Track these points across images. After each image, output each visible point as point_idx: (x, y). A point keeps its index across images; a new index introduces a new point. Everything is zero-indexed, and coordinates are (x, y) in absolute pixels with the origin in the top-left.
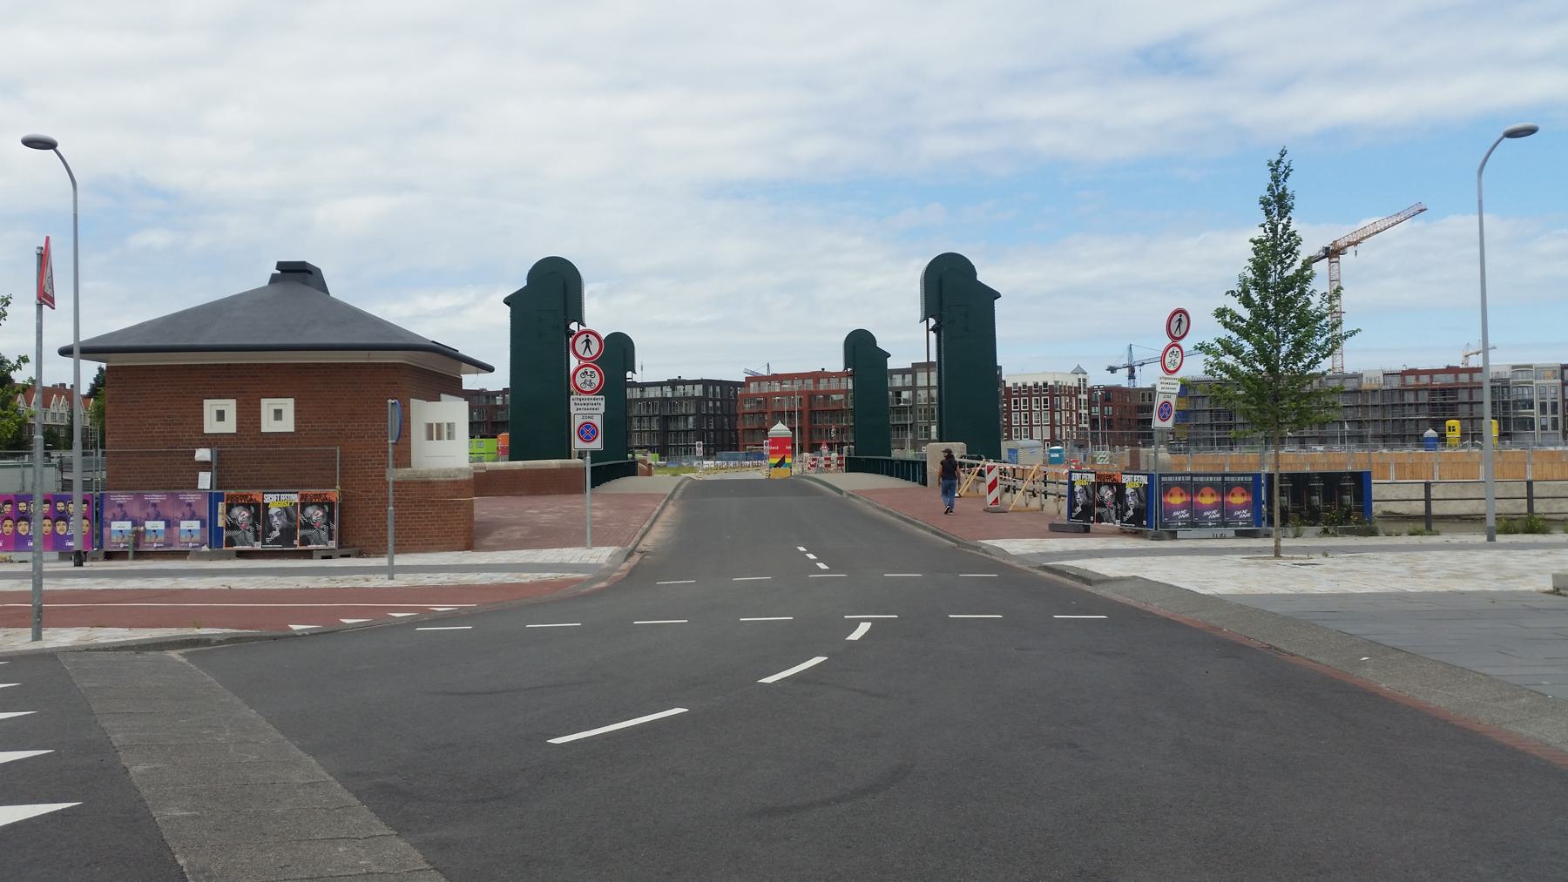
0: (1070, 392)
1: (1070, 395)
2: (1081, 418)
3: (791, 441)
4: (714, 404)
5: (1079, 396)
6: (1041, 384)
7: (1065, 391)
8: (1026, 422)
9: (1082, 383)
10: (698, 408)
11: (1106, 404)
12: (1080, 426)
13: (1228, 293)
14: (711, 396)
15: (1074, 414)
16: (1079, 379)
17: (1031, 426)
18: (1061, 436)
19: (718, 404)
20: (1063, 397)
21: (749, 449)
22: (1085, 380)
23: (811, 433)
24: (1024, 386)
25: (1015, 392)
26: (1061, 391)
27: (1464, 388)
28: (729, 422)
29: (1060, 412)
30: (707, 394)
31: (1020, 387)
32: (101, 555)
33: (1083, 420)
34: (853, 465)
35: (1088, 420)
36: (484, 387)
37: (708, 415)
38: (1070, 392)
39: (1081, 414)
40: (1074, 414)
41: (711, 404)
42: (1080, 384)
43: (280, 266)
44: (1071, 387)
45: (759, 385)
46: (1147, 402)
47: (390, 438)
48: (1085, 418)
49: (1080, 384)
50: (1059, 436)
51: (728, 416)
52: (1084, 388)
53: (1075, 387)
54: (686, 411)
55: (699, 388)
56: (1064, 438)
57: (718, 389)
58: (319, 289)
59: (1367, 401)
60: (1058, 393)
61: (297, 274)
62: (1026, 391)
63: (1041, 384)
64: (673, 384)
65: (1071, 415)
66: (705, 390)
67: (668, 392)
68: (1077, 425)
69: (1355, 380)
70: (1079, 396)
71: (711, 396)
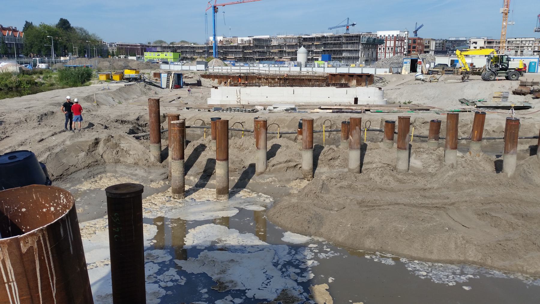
6: (391, 35)
24: (393, 36)
31: (391, 37)
38: (402, 39)
46: (428, 44)
62: (393, 38)
63: (391, 35)
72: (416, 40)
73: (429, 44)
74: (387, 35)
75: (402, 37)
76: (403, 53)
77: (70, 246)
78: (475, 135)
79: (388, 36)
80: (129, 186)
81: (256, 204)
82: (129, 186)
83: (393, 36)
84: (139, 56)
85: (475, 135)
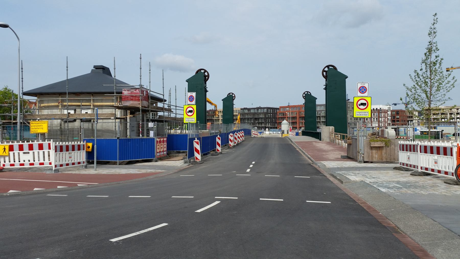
1: (385, 112)
2: (388, 120)
4: (270, 115)
5: (388, 113)
6: (375, 109)
7: (383, 111)
9: (389, 108)
10: (265, 116)
11: (394, 115)
14: (269, 112)
16: (388, 107)
17: (372, 122)
18: (382, 125)
19: (271, 115)
23: (299, 123)
24: (377, 109)
27: (97, 112)
28: (275, 120)
29: (381, 118)
30: (268, 111)
31: (375, 110)
33: (389, 120)
34: (304, 133)
35: (391, 120)
36: (402, 109)
37: (268, 118)
38: (385, 111)
39: (388, 118)
41: (269, 115)
42: (388, 109)
43: (95, 67)
44: (385, 110)
47: (203, 124)
48: (390, 120)
49: (388, 109)
50: (381, 125)
51: (274, 118)
52: (390, 110)
54: (262, 116)
55: (265, 110)
56: (383, 126)
57: (271, 110)
58: (108, 74)
59: (245, 117)
61: (104, 70)
63: (375, 109)
64: (258, 109)
65: (385, 119)
66: (268, 110)
67: (256, 111)
70: (388, 113)
71: (269, 112)
72: (399, 111)
73: (286, 116)
74: (379, 108)
75: (385, 110)
76: (387, 122)
77: (72, 174)
78: (165, 171)
79: (373, 109)
80: (21, 169)
81: (398, 159)
82: (21, 169)
83: (377, 109)
84: (180, 127)
85: (165, 171)
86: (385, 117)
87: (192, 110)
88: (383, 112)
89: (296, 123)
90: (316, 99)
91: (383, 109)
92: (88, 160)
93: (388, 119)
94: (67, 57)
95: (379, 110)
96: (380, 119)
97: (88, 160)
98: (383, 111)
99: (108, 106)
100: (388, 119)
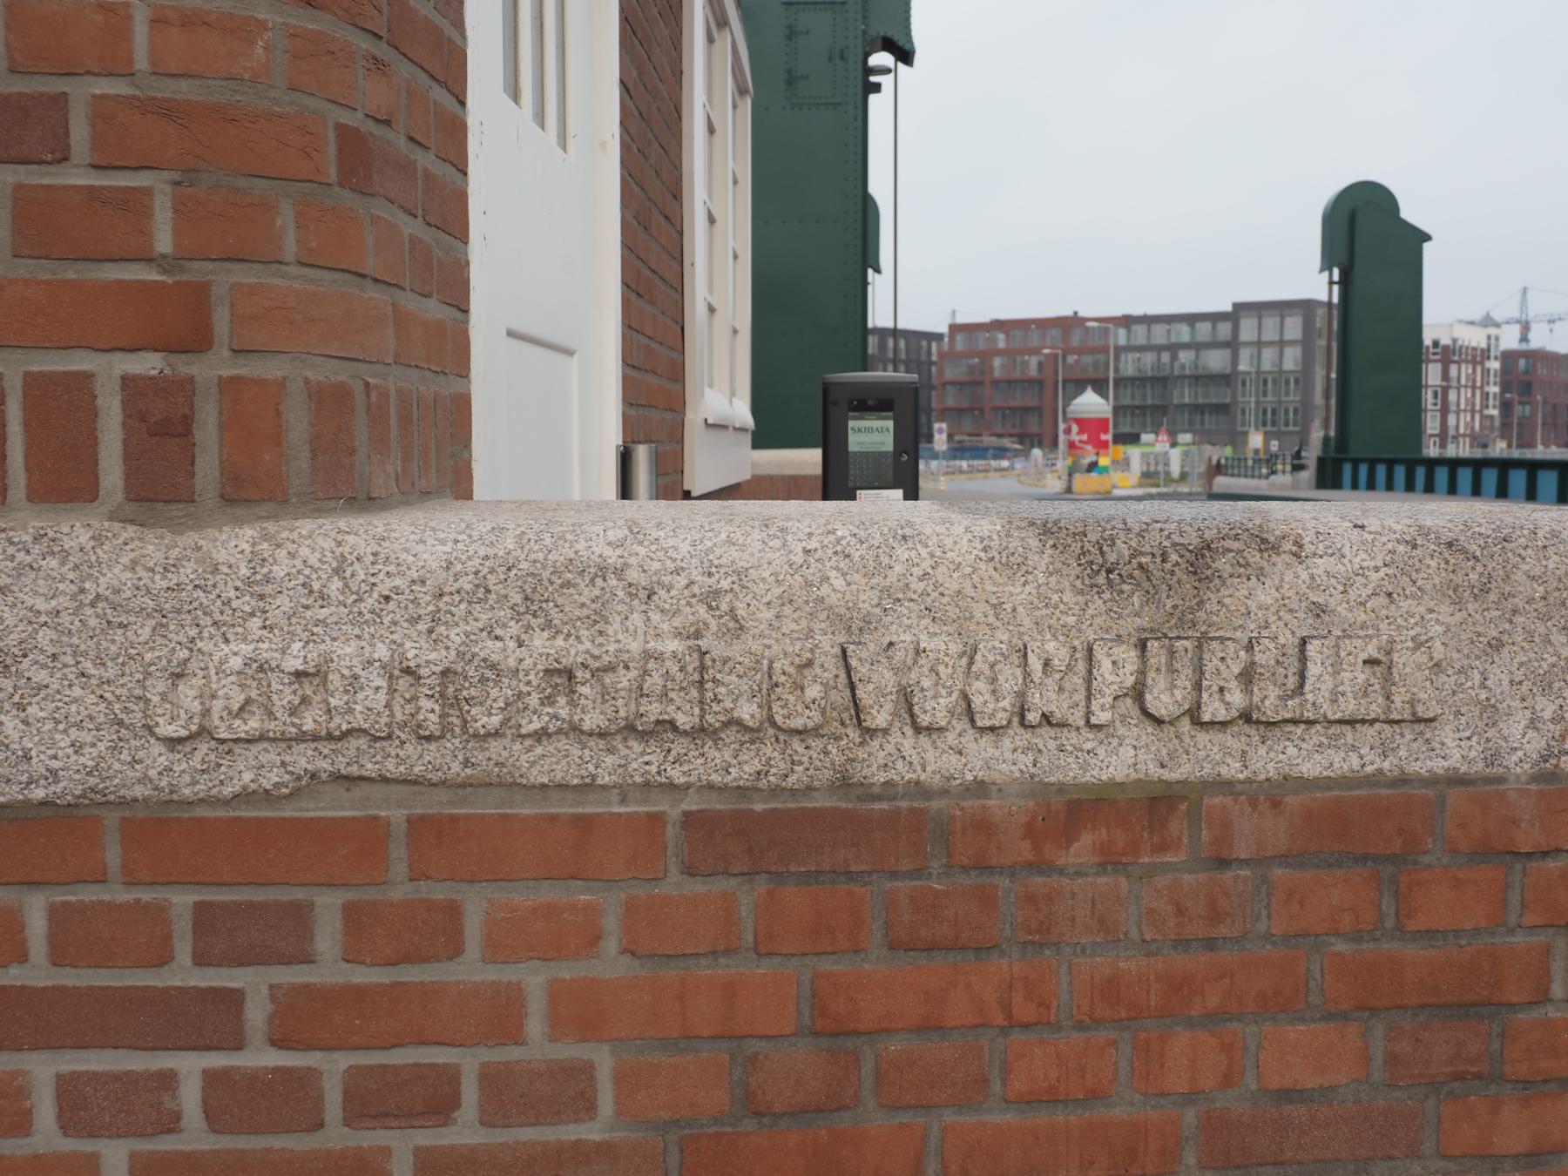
0: (1474, 357)
1: (1474, 362)
2: (1487, 399)
3: (1102, 424)
7: (1467, 354)
8: (1436, 404)
12: (1486, 412)
13: (807, 32)
15: (1478, 393)
16: (1489, 337)
20: (1463, 366)
21: (959, 442)
22: (1497, 339)
25: (1434, 354)
26: (1460, 355)
29: (1458, 389)
32: (680, 494)
35: (1497, 403)
38: (1474, 357)
39: (1488, 394)
40: (1478, 393)
42: (1489, 345)
45: (1149, 330)
49: (1489, 345)
53: (1482, 350)
57: (902, 343)
60: (1456, 358)
68: (1481, 412)
69: (1216, 489)
71: (891, 355)
75: (1475, 349)
86: (1474, 387)
87: (133, 1155)
88: (1467, 361)
89: (1040, 417)
90: (1427, 238)
91: (1466, 343)
92: (113, 855)
93: (1485, 396)
94: (511, 334)
95: (1446, 348)
96: (1452, 396)
97: (113, 855)
98: (1467, 354)
99: (563, 41)
100: (1485, 396)
